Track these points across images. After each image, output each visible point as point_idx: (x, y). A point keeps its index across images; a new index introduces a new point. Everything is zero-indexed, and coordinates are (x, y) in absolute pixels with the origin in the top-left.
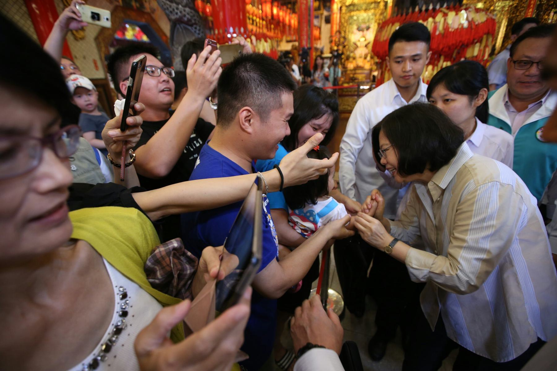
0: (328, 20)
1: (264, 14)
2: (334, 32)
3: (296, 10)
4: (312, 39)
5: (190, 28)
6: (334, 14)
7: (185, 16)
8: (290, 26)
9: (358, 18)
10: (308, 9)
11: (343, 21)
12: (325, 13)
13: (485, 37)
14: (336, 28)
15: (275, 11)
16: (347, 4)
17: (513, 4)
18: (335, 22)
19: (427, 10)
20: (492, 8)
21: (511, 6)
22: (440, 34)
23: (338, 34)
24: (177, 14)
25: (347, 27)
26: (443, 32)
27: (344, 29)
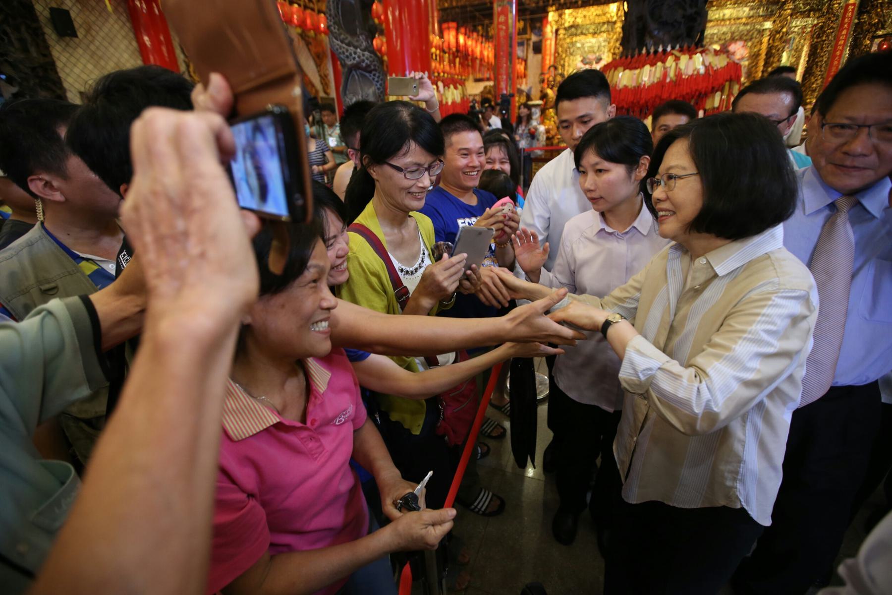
0: (538, 49)
1: (446, 44)
2: (547, 66)
3: (492, 32)
4: (514, 77)
5: (367, 74)
6: (546, 40)
7: (363, 61)
8: (482, 60)
9: (583, 44)
10: (510, 38)
11: (560, 50)
12: (534, 38)
13: (727, 84)
14: (549, 60)
15: (461, 39)
16: (567, 25)
17: (818, 24)
18: (548, 52)
19: (656, 52)
20: (784, 30)
21: (815, 25)
22: (671, 81)
23: (552, 69)
24: (354, 58)
25: (567, 59)
26: (674, 79)
27: (562, 62)
